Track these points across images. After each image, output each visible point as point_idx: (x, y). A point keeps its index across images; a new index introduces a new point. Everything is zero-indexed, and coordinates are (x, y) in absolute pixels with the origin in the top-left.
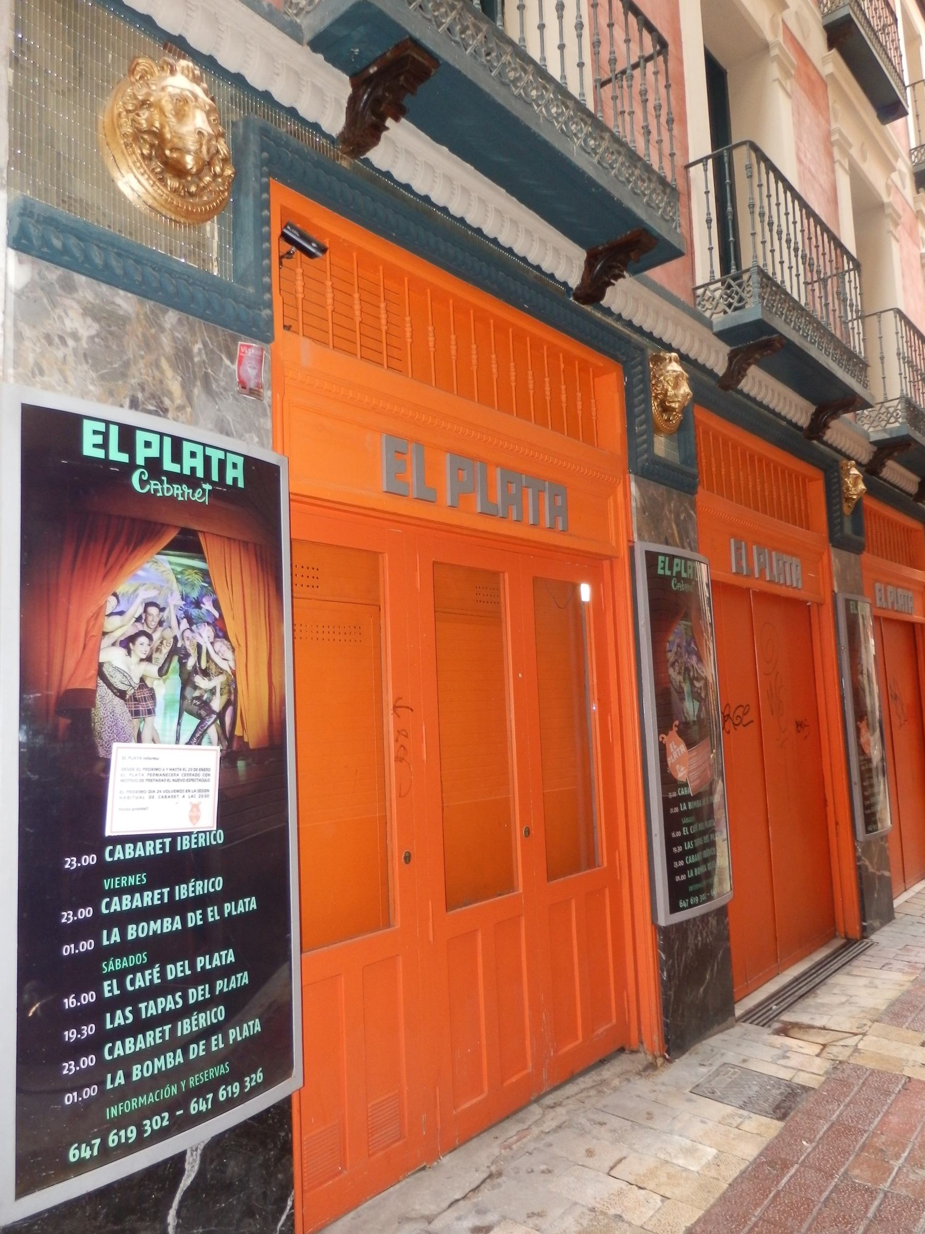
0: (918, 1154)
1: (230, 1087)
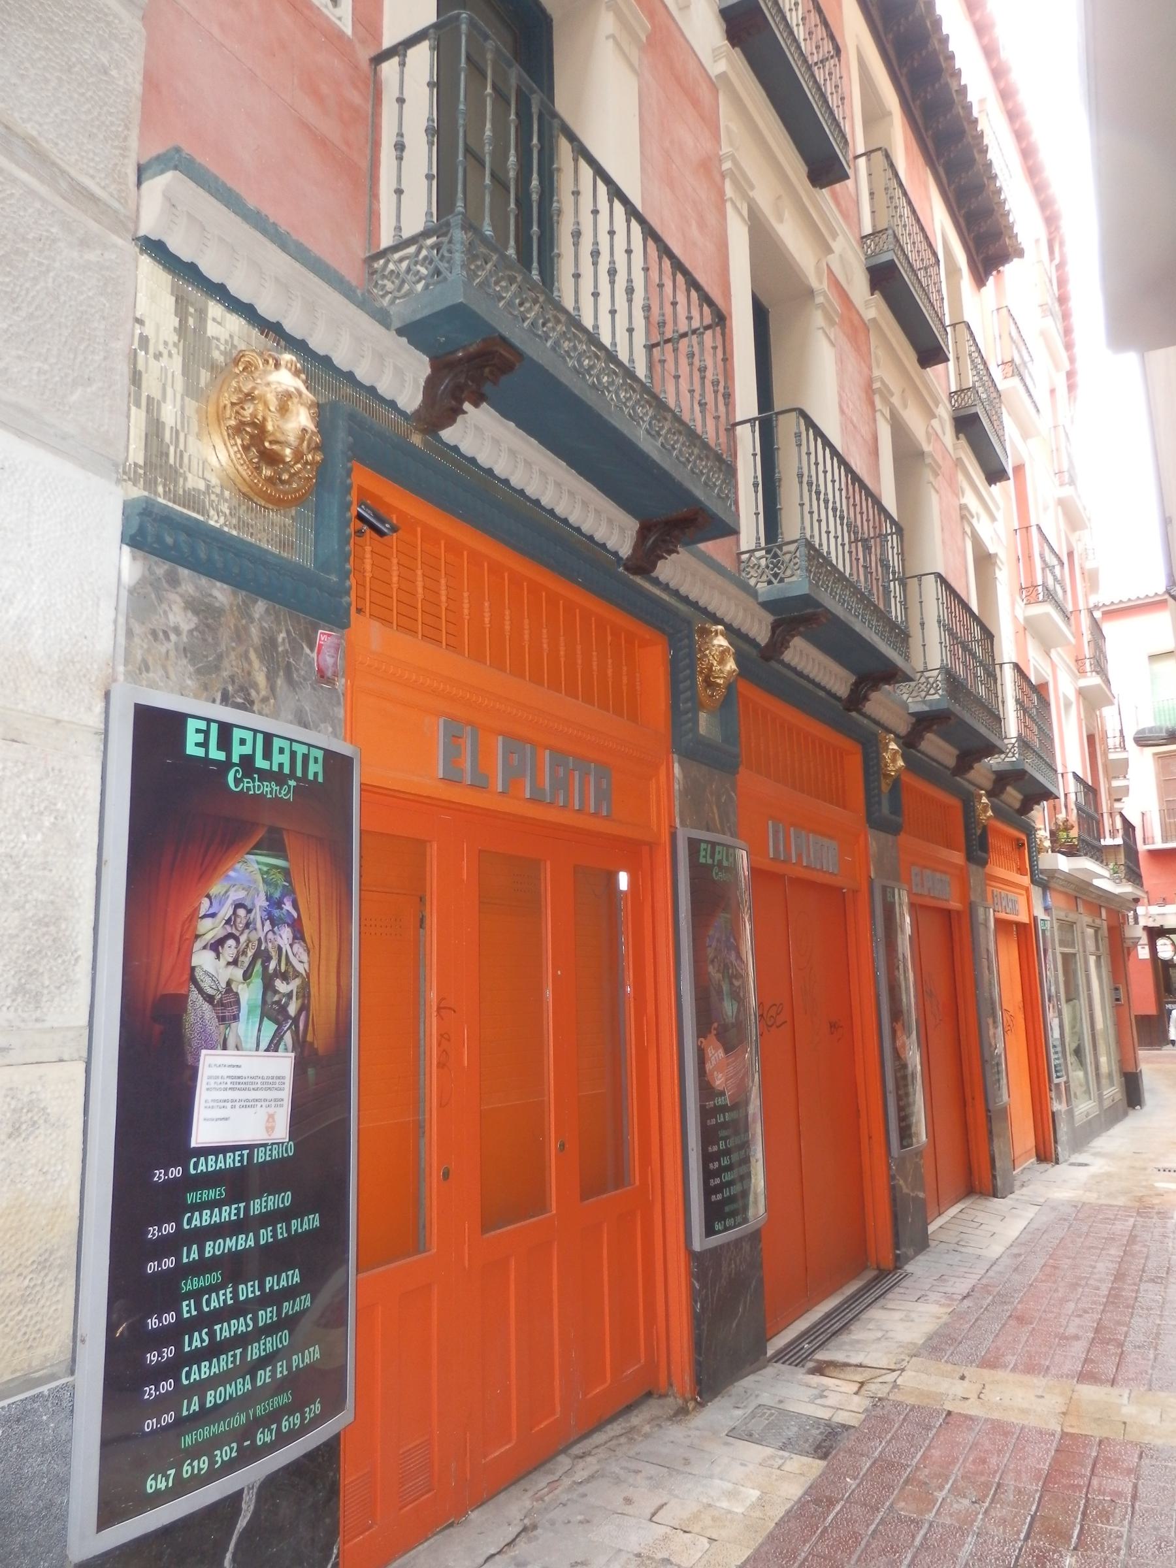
0: (961, 1484)
1: (196, 1462)
